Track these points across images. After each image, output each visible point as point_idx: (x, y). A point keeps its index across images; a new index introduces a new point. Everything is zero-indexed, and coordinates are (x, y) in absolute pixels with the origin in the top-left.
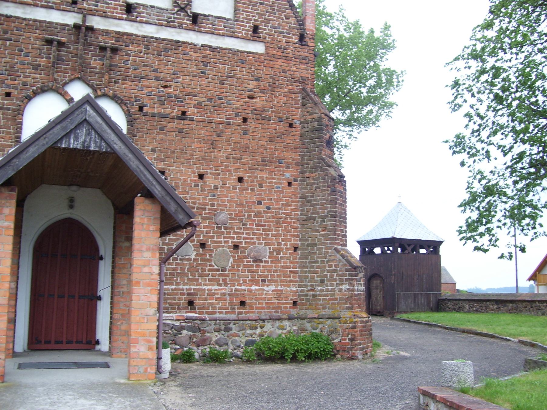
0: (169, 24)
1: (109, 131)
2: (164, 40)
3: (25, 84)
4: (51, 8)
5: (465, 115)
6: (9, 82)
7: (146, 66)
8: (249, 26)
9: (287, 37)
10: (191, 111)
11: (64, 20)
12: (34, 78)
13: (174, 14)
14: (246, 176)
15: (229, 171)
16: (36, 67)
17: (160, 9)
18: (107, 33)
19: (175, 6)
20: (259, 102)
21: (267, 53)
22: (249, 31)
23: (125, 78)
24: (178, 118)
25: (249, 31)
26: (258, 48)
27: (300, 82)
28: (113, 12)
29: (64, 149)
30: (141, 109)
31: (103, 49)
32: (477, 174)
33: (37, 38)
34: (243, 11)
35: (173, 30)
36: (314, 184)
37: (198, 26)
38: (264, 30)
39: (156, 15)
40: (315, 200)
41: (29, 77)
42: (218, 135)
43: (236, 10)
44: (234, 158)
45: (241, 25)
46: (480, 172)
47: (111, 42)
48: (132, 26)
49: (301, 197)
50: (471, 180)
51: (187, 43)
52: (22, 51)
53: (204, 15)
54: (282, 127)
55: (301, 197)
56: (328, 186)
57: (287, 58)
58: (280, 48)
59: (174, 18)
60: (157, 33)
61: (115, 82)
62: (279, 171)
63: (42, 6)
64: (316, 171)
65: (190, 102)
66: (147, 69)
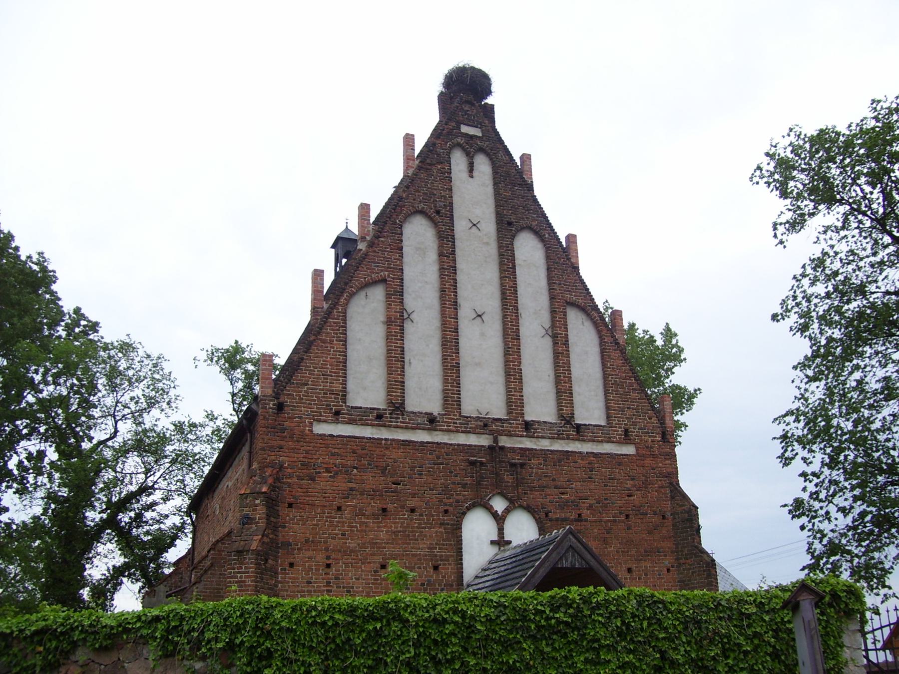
0: (559, 437)
1: (586, 553)
2: (557, 451)
3: (458, 501)
4: (469, 432)
5: (801, 475)
6: (445, 501)
7: (547, 476)
8: (621, 431)
9: (652, 436)
10: (586, 513)
11: (479, 442)
12: (464, 496)
13: (562, 427)
14: (634, 566)
15: (620, 564)
16: (464, 486)
17: (551, 423)
18: (513, 450)
19: (562, 420)
20: (637, 499)
21: (638, 453)
22: (622, 435)
23: (532, 489)
24: (576, 520)
25: (622, 435)
26: (630, 450)
27: (666, 477)
28: (515, 431)
29: (561, 568)
30: (547, 515)
31: (513, 465)
32: (817, 533)
33: (462, 461)
34: (615, 417)
35: (562, 442)
36: (690, 569)
37: (582, 436)
38: (634, 432)
39: (549, 430)
40: (693, 584)
41: (460, 494)
42: (608, 533)
43: (608, 417)
44: (622, 552)
45: (615, 431)
46: (820, 531)
47: (517, 460)
48: (531, 441)
49: (678, 582)
50: (810, 540)
51: (575, 452)
52: (452, 472)
53: (585, 425)
54: (656, 520)
55: (678, 582)
56: (704, 571)
57: (654, 456)
58: (647, 447)
59: (563, 431)
60: (551, 445)
61: (525, 493)
62: (659, 560)
63: (463, 432)
64: (691, 558)
65: (583, 505)
66: (548, 478)
